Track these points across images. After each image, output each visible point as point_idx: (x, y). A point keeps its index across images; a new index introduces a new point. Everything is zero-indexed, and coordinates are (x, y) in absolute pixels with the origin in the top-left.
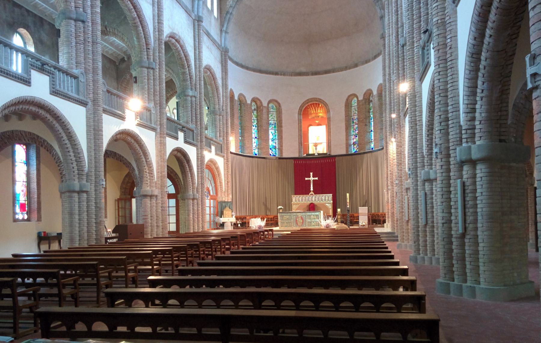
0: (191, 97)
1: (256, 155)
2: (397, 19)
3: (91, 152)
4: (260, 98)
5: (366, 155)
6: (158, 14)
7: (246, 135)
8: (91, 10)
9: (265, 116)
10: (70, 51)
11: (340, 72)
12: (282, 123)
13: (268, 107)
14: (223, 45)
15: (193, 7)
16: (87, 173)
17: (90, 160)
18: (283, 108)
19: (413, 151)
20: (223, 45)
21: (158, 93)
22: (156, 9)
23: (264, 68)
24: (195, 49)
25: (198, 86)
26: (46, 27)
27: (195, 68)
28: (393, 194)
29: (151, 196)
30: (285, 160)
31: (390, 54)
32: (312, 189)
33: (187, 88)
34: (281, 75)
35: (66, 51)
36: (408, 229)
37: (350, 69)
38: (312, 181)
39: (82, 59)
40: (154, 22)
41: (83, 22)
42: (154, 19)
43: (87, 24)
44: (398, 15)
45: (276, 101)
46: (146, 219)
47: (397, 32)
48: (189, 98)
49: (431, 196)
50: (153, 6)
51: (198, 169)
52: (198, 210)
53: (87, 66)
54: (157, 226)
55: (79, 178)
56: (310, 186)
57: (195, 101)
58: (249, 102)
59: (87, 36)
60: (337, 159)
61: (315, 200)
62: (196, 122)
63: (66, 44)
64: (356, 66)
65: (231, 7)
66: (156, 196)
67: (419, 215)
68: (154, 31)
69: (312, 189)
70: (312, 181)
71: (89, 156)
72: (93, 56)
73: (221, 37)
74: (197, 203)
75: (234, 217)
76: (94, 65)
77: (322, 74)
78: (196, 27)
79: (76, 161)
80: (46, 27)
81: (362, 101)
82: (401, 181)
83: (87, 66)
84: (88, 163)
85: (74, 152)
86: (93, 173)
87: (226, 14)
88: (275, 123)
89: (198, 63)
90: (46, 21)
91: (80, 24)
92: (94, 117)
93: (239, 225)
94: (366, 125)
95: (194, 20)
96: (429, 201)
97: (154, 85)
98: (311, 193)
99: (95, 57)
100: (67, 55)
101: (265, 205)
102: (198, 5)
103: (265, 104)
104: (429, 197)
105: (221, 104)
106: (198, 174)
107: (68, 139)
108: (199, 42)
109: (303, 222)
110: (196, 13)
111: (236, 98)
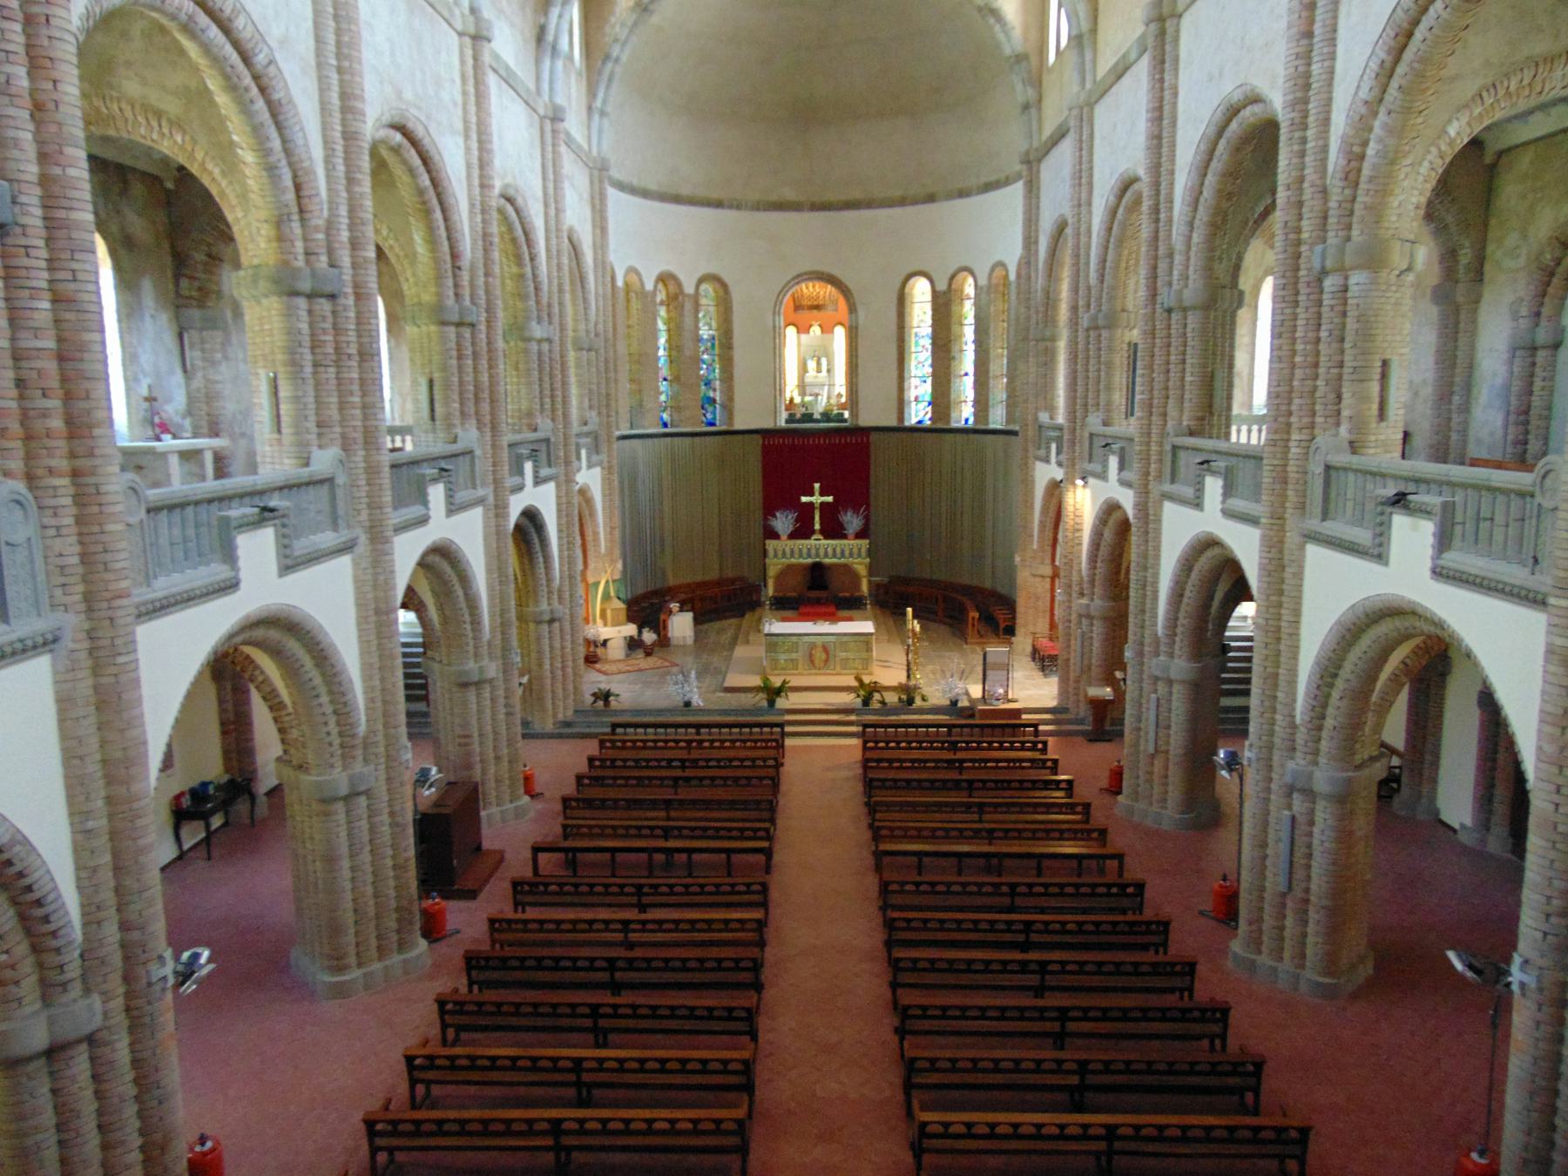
0: (540, 341)
1: (665, 425)
6: (480, 159)
8: (352, 257)
10: (300, 393)
13: (696, 298)
14: (595, 152)
15: (538, 78)
16: (365, 738)
19: (1267, 704)
20: (595, 152)
21: (486, 395)
22: (474, 145)
23: (685, 191)
24: (546, 205)
26: (138, 189)
27: (549, 257)
29: (478, 684)
30: (740, 437)
32: (817, 526)
33: (528, 319)
34: (731, 207)
36: (1151, 773)
39: (334, 413)
40: (470, 185)
41: (332, 297)
42: (469, 176)
43: (342, 301)
44: (1157, 221)
46: (466, 745)
47: (1155, 268)
48: (534, 347)
49: (1307, 828)
50: (467, 137)
51: (560, 538)
52: (563, 648)
54: (498, 758)
55: (344, 757)
58: (649, 286)
62: (553, 410)
64: (931, 198)
66: (491, 681)
67: (1268, 863)
68: (471, 212)
69: (817, 526)
71: (368, 690)
72: (364, 395)
73: (589, 128)
74: (561, 630)
78: (549, 136)
79: (335, 712)
80: (138, 189)
85: (331, 692)
86: (380, 738)
88: (713, 338)
90: (134, 170)
91: (324, 306)
92: (375, 575)
95: (542, 118)
96: (1300, 841)
99: (367, 399)
102: (552, 72)
103: (689, 289)
104: (1302, 828)
105: (592, 317)
106: (561, 551)
107: (317, 665)
108: (555, 181)
109: (827, 661)
110: (546, 97)
111: (620, 283)
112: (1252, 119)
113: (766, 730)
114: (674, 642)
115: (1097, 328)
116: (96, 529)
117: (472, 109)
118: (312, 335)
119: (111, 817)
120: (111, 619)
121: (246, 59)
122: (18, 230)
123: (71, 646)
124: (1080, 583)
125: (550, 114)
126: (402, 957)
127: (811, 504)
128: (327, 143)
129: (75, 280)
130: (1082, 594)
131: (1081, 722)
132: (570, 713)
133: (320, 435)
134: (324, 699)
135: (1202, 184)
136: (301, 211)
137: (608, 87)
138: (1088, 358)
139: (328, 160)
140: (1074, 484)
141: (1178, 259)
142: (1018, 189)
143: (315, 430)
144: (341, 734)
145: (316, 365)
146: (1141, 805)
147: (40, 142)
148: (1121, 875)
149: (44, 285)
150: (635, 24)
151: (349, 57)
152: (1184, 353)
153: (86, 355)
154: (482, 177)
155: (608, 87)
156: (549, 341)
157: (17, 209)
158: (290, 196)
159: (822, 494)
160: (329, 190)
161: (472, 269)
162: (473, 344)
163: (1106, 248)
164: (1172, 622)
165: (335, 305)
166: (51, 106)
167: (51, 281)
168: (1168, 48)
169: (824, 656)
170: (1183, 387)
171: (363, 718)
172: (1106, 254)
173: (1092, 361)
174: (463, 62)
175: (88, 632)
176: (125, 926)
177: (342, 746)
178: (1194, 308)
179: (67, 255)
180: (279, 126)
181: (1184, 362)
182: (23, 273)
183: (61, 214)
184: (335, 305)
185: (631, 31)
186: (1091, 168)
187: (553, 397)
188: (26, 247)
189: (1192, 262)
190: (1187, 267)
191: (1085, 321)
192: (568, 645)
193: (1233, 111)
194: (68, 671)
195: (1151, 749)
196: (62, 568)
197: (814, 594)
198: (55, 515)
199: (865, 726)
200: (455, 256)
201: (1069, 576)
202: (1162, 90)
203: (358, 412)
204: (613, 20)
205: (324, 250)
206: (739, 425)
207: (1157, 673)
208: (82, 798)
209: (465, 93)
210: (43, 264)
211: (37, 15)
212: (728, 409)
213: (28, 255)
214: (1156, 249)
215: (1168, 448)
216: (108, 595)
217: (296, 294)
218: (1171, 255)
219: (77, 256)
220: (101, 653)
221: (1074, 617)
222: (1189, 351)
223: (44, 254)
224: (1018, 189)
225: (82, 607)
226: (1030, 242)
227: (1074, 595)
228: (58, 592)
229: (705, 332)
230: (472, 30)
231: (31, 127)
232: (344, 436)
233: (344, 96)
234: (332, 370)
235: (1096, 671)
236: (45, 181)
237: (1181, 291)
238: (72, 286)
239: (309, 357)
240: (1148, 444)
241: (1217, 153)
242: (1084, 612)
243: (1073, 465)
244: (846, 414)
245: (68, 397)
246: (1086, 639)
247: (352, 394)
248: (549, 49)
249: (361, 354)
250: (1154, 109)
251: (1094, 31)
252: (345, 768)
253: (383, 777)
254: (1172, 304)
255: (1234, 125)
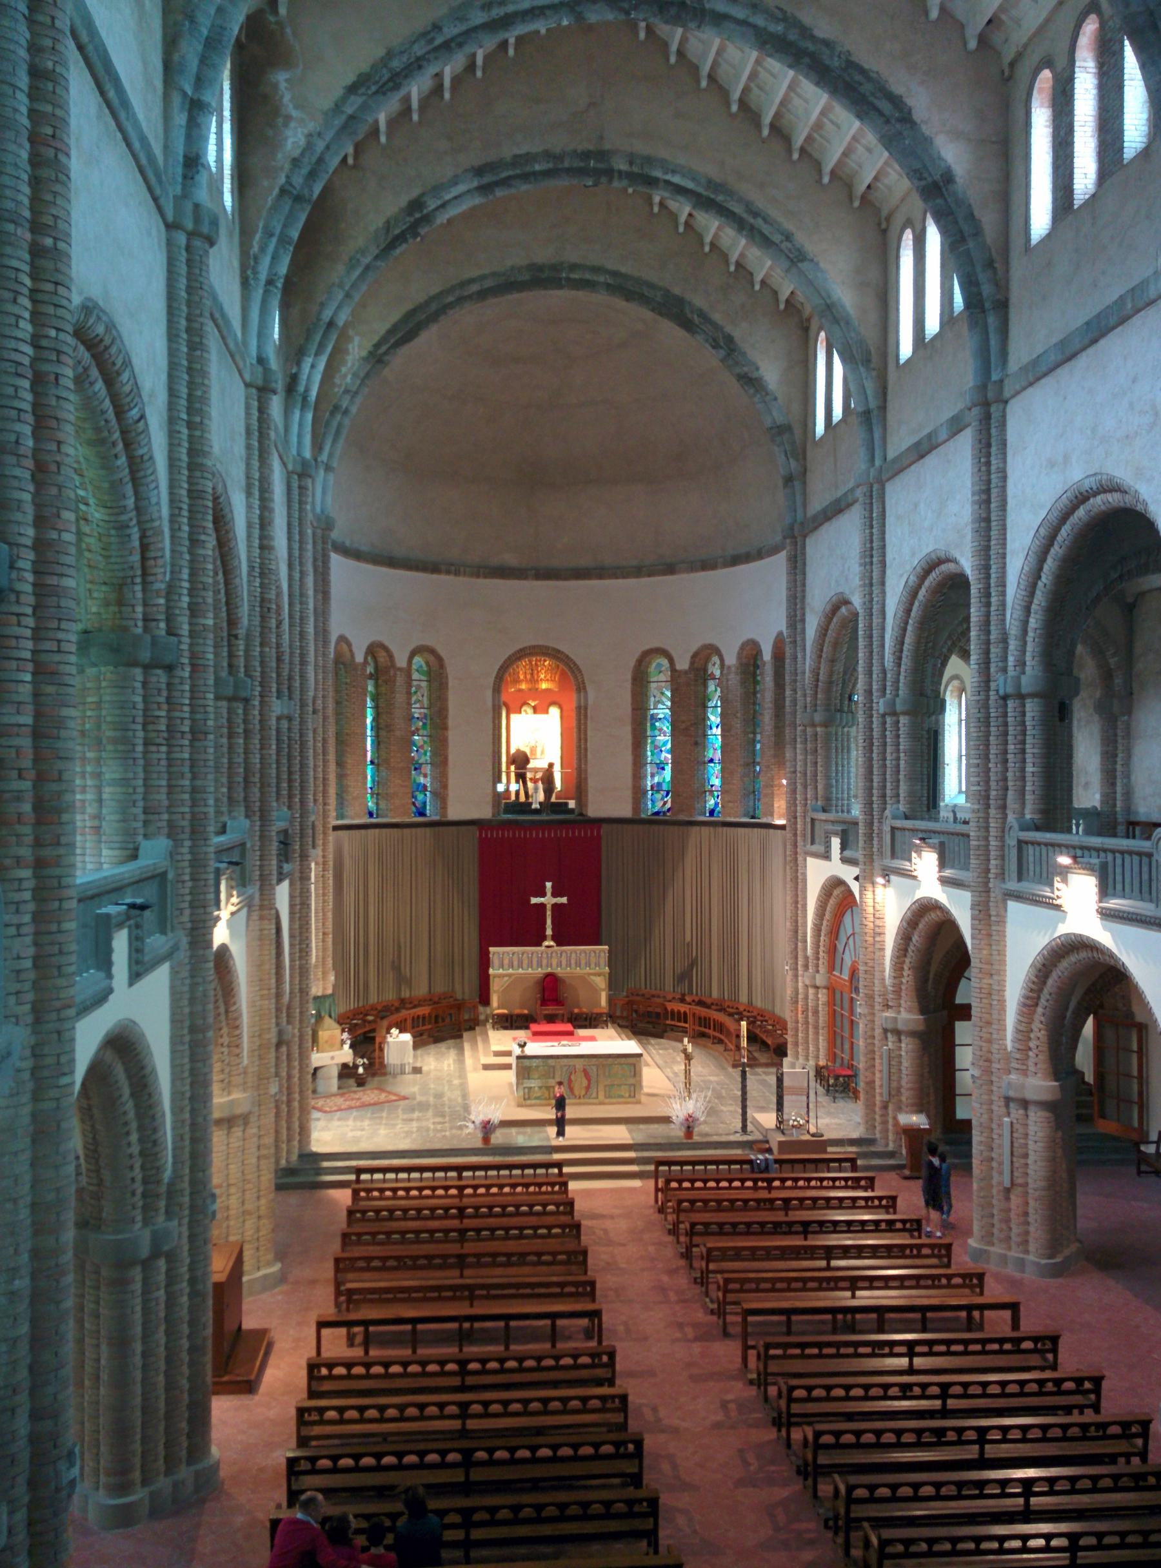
1: (371, 814)
2: (988, 615)
3: (182, 1110)
4: (387, 643)
5: (695, 829)
6: (261, 517)
7: (350, 760)
9: (400, 698)
10: (131, 775)
11: (620, 581)
12: (446, 717)
13: (408, 672)
17: (178, 1138)
18: (452, 671)
21: (257, 779)
25: (297, 684)
28: (873, 1029)
30: (453, 829)
31: (871, 637)
32: (549, 932)
34: (448, 572)
35: (117, 776)
37: (649, 576)
38: (549, 907)
41: (170, 668)
43: (178, 672)
45: (432, 651)
53: (175, 817)
56: (545, 923)
57: (289, 729)
59: (177, 714)
60: (605, 828)
61: (560, 964)
62: (290, 796)
63: (116, 751)
65: (346, 391)
69: (549, 932)
70: (549, 907)
72: (194, 777)
74: (289, 1055)
75: (346, 1047)
76: (196, 809)
77: (566, 579)
78: (296, 492)
81: (686, 672)
82: (988, 1072)
83: (175, 817)
84: (174, 1149)
87: (332, 413)
88: (425, 716)
89: (297, 608)
93: (361, 1070)
94: (696, 744)
97: (247, 752)
98: (546, 943)
99: (199, 783)
100: (119, 789)
101: (397, 968)
109: (588, 1088)
112: (1103, 508)
113: (503, 1172)
114: (390, 1069)
115: (894, 714)
116: (54, 927)
117: (256, 464)
118: (145, 710)
119: (34, 1276)
120: (59, 1033)
121: (120, 412)
122: (13, 597)
123: (18, 1064)
124: (884, 995)
125: (299, 469)
126: (193, 1468)
127: (543, 906)
128: (173, 501)
129: (59, 651)
130: (888, 1007)
131: (892, 1155)
132: (294, 1157)
133: (146, 823)
134: (134, 1137)
135: (1040, 569)
136: (145, 574)
137: (335, 441)
138: (885, 744)
139: (173, 518)
140: (873, 883)
141: (1013, 645)
142: (781, 558)
143: (142, 817)
144: (145, 1182)
145: (147, 743)
146: (997, 1249)
147: (38, 505)
148: (1015, 1325)
149: (28, 655)
150: (367, 375)
151: (200, 412)
152: (1023, 742)
153: (63, 733)
154: (261, 538)
155: (335, 441)
156: (290, 719)
157: (14, 575)
158: (136, 558)
159: (554, 895)
160: (173, 551)
161: (248, 637)
162: (245, 721)
163: (905, 630)
164: (1023, 1034)
165: (171, 677)
166: (53, 468)
167: (34, 652)
168: (993, 431)
169: (585, 1083)
170: (1023, 778)
171: (170, 1160)
172: (903, 636)
173: (889, 749)
174: (248, 414)
175: (33, 1048)
176: (36, 1416)
177: (144, 1195)
178: (1032, 695)
179: (55, 624)
180: (135, 481)
181: (1023, 751)
182: (13, 643)
183: (53, 580)
184: (171, 677)
185: (363, 381)
186: (884, 547)
187: (290, 781)
188: (18, 615)
189: (1029, 648)
190: (1024, 652)
191: (880, 706)
192: (296, 1072)
193: (1081, 498)
194: (12, 1096)
195: (1007, 1184)
196: (18, 972)
197: (550, 1010)
198: (17, 911)
199: (659, 1163)
200: (232, 622)
201: (870, 986)
202: (989, 472)
203: (186, 796)
204: (344, 370)
205: (163, 617)
206: (455, 812)
207: (1012, 1094)
208: (11, 1250)
209: (249, 447)
210: (28, 633)
211: (48, 373)
212: (441, 796)
213: (19, 625)
214: (988, 632)
215: (1013, 842)
216: (57, 1004)
217: (135, 664)
218: (1004, 640)
219: (64, 625)
220: (46, 1073)
221: (878, 1032)
222: (1029, 740)
223: (30, 622)
224: (781, 558)
225: (29, 1019)
226: (796, 619)
227: (877, 1007)
228: (12, 1000)
229: (417, 712)
230: (260, 382)
231: (31, 488)
232: (171, 825)
233: (192, 452)
234: (164, 749)
235: (906, 1096)
236: (40, 545)
237: (1018, 679)
238: (57, 658)
239: (141, 734)
240: (986, 839)
241: (1059, 538)
242: (889, 1026)
243: (872, 861)
244: (572, 804)
245: (40, 779)
246: (893, 1059)
247: (183, 775)
248: (300, 399)
249: (192, 731)
250: (981, 492)
251: (883, 408)
252: (146, 1222)
253: (186, 1233)
254: (1010, 690)
255: (1081, 512)
